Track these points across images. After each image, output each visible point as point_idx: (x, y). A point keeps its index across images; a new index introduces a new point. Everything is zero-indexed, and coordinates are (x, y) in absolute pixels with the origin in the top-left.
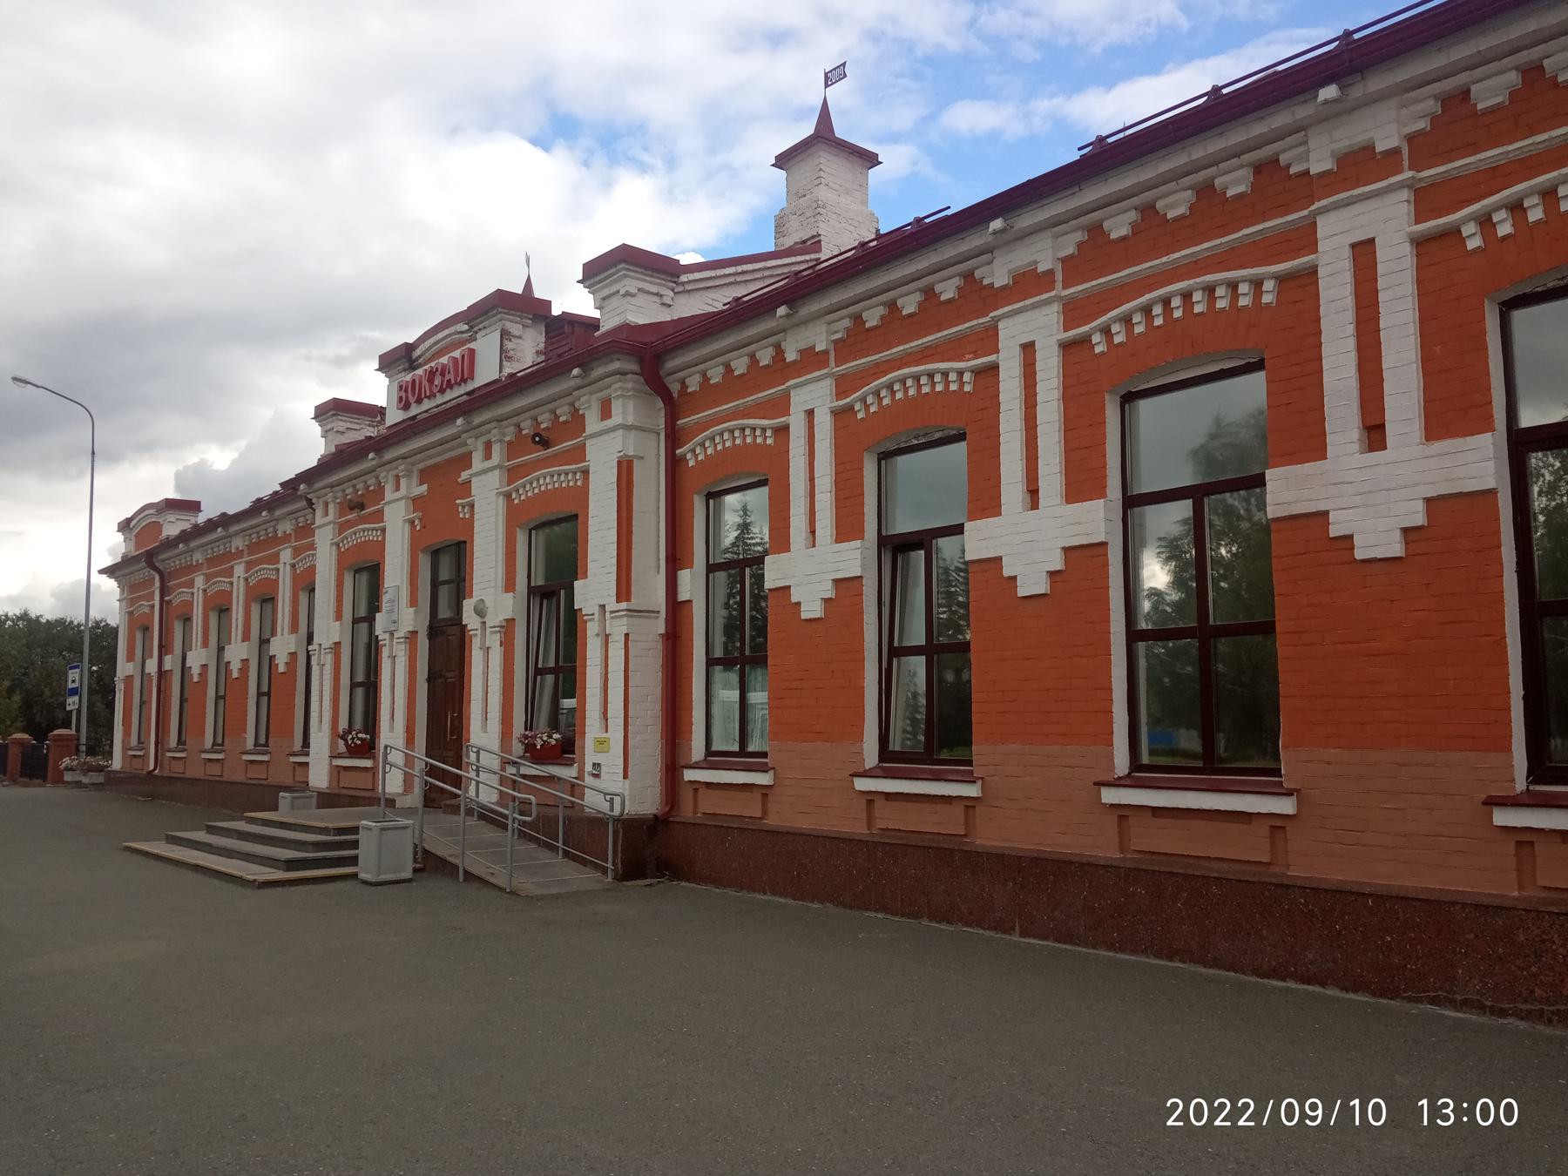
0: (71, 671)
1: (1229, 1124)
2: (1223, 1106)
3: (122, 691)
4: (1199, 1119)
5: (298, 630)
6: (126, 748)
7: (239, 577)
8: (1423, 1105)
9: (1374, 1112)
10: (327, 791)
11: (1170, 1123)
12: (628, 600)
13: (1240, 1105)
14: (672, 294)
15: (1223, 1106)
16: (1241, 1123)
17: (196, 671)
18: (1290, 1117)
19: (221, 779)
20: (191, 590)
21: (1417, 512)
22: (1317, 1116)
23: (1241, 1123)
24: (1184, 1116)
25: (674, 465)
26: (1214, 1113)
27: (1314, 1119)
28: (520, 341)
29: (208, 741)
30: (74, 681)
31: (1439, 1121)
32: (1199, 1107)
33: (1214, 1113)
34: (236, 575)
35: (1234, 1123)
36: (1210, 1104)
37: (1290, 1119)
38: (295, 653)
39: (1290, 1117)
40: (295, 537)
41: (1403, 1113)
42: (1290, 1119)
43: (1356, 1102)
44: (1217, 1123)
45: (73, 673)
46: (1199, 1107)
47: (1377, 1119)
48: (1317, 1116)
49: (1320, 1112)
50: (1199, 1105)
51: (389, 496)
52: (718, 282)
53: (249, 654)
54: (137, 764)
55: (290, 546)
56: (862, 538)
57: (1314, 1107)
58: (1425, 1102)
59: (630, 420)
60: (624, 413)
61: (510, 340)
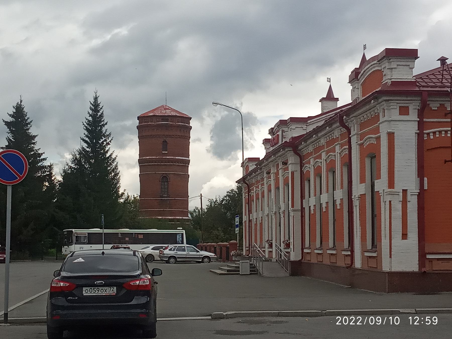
0: (236, 218)
1: (354, 324)
2: (353, 319)
3: (358, 206)
4: (346, 322)
5: (381, 178)
6: (364, 250)
7: (337, 152)
8: (410, 319)
9: (396, 320)
10: (361, 268)
11: (337, 324)
12: (293, 207)
13: (357, 318)
14: (306, 126)
15: (353, 319)
16: (358, 324)
17: (324, 206)
18: (372, 322)
19: (375, 270)
20: (334, 154)
21: (300, 210)
22: (380, 322)
23: (358, 324)
24: (341, 322)
25: (302, 172)
26: (350, 321)
27: (379, 322)
28: (287, 132)
29: (331, 245)
30: (237, 222)
31: (426, 323)
32: (346, 319)
33: (350, 321)
34: (336, 152)
35: (356, 324)
36: (349, 319)
37: (372, 322)
38: (343, 199)
39: (372, 322)
40: (314, 153)
41: (405, 322)
42: (372, 322)
43: (391, 318)
44: (351, 324)
45: (237, 219)
46: (346, 319)
47: (397, 322)
48: (380, 322)
49: (380, 320)
50: (346, 319)
51: (381, 119)
52: (321, 120)
53: (256, 217)
54: (373, 264)
55: (313, 157)
56: (365, 183)
57: (379, 319)
58: (411, 318)
59: (293, 162)
60: (292, 160)
61: (285, 133)
